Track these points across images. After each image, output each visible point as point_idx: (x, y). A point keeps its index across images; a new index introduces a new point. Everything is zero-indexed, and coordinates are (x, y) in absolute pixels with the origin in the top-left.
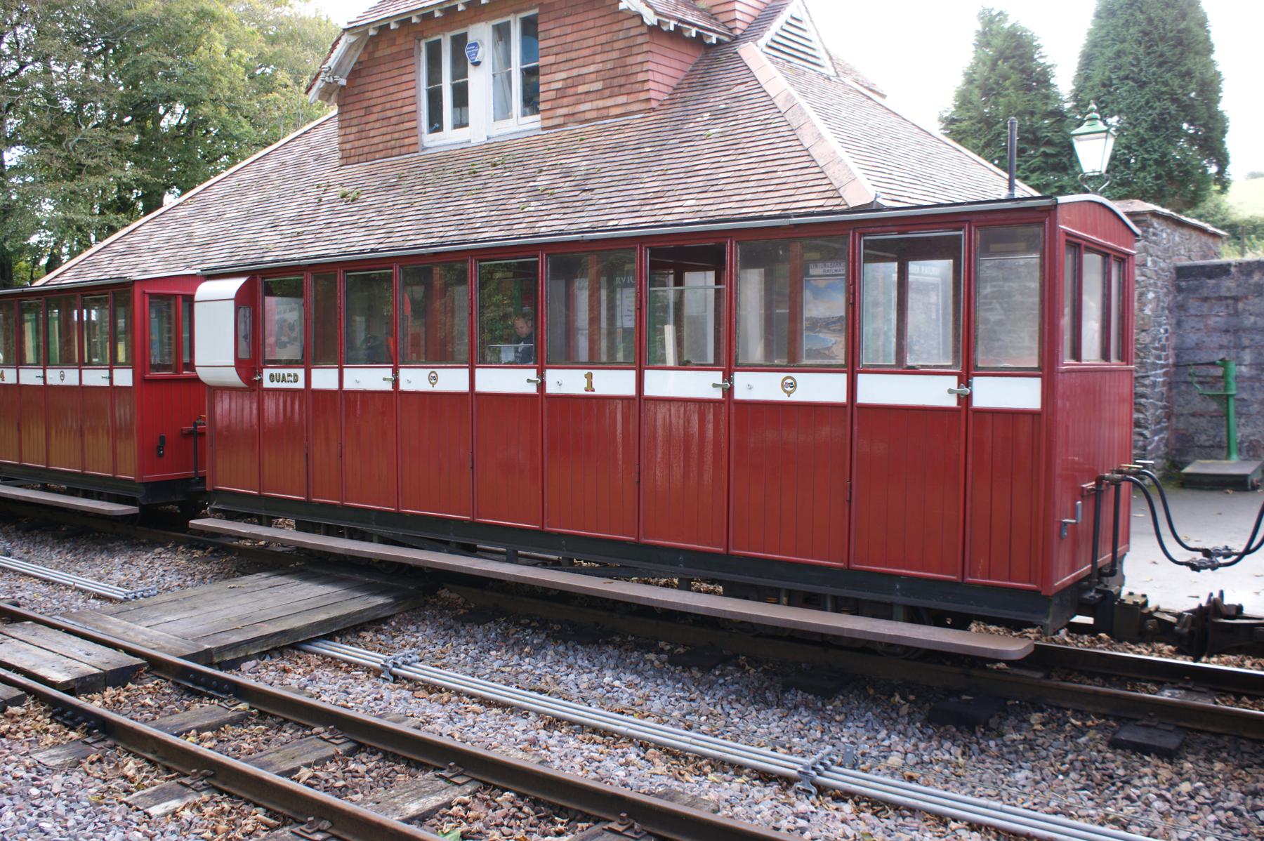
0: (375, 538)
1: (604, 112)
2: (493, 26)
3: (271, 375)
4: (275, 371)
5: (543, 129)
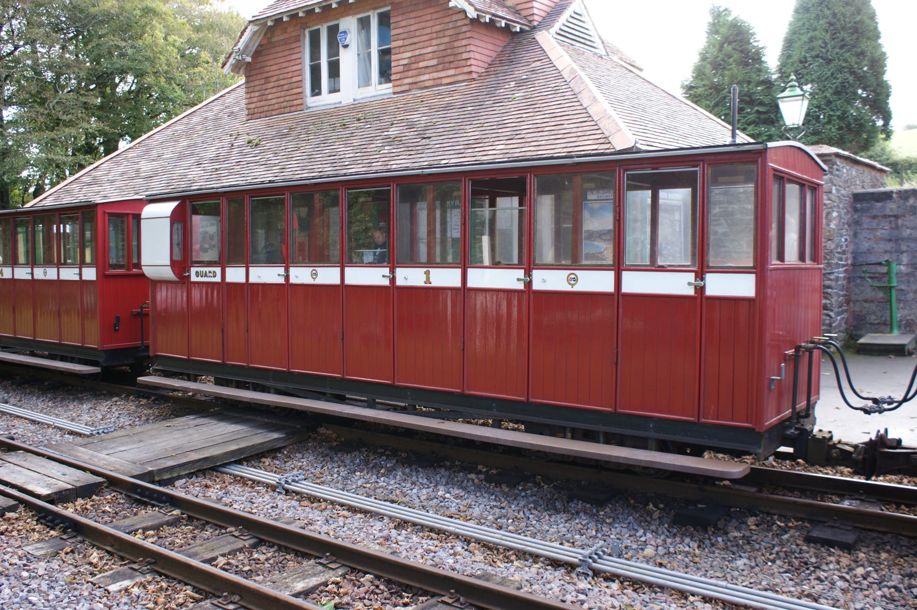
0: (272, 390)
1: (438, 82)
2: (358, 19)
3: (197, 272)
4: (199, 269)
5: (394, 93)
